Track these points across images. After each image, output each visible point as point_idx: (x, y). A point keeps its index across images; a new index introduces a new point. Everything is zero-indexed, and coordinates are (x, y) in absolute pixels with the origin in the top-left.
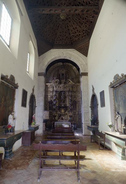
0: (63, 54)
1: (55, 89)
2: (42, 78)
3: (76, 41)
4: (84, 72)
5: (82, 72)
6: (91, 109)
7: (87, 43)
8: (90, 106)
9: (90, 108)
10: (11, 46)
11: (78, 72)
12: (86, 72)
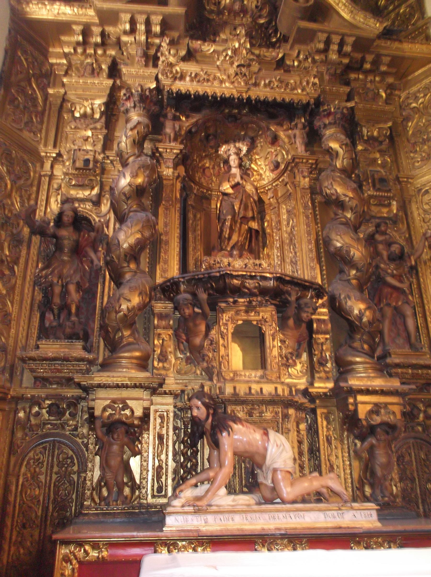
1: (138, 76)
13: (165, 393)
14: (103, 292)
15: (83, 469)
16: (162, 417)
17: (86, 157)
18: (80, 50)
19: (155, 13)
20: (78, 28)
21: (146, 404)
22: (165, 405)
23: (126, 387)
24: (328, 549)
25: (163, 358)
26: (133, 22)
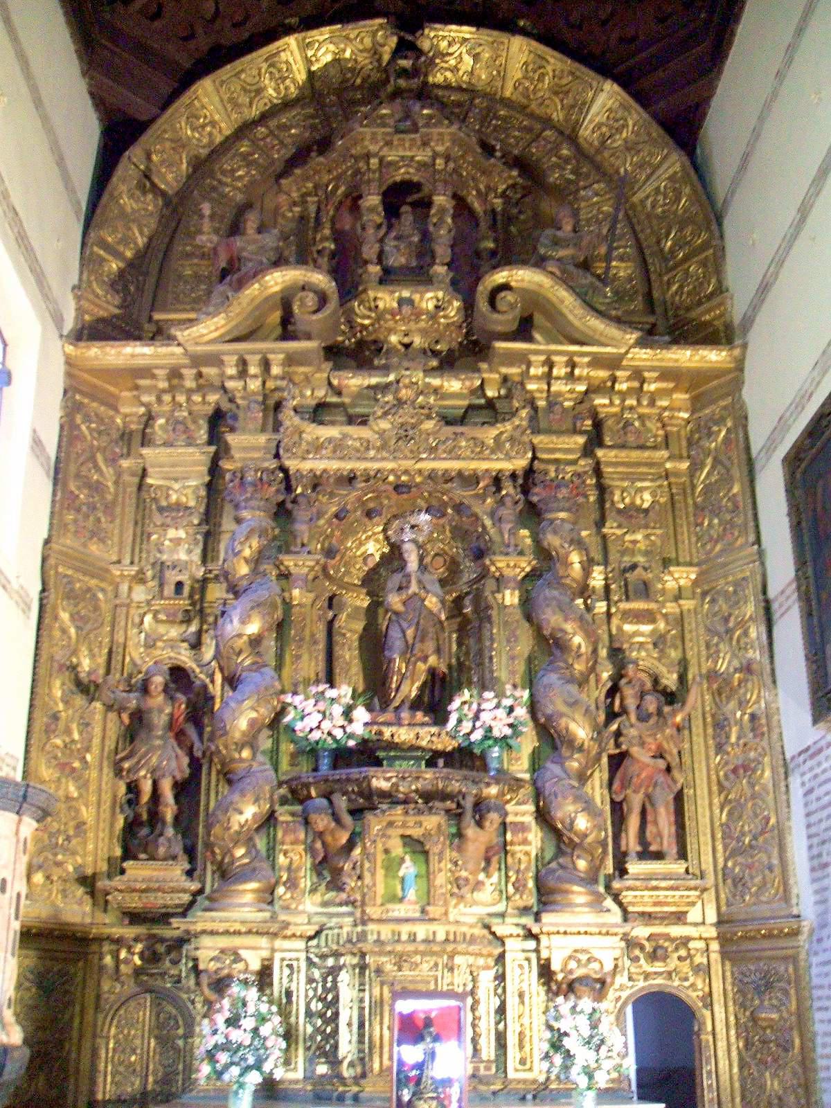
11: (675, 162)
13: (294, 935)
14: (209, 782)
16: (290, 966)
17: (179, 578)
19: (273, 352)
20: (161, 373)
21: (265, 954)
24: (730, 43)
25: (292, 884)
26: (243, 363)
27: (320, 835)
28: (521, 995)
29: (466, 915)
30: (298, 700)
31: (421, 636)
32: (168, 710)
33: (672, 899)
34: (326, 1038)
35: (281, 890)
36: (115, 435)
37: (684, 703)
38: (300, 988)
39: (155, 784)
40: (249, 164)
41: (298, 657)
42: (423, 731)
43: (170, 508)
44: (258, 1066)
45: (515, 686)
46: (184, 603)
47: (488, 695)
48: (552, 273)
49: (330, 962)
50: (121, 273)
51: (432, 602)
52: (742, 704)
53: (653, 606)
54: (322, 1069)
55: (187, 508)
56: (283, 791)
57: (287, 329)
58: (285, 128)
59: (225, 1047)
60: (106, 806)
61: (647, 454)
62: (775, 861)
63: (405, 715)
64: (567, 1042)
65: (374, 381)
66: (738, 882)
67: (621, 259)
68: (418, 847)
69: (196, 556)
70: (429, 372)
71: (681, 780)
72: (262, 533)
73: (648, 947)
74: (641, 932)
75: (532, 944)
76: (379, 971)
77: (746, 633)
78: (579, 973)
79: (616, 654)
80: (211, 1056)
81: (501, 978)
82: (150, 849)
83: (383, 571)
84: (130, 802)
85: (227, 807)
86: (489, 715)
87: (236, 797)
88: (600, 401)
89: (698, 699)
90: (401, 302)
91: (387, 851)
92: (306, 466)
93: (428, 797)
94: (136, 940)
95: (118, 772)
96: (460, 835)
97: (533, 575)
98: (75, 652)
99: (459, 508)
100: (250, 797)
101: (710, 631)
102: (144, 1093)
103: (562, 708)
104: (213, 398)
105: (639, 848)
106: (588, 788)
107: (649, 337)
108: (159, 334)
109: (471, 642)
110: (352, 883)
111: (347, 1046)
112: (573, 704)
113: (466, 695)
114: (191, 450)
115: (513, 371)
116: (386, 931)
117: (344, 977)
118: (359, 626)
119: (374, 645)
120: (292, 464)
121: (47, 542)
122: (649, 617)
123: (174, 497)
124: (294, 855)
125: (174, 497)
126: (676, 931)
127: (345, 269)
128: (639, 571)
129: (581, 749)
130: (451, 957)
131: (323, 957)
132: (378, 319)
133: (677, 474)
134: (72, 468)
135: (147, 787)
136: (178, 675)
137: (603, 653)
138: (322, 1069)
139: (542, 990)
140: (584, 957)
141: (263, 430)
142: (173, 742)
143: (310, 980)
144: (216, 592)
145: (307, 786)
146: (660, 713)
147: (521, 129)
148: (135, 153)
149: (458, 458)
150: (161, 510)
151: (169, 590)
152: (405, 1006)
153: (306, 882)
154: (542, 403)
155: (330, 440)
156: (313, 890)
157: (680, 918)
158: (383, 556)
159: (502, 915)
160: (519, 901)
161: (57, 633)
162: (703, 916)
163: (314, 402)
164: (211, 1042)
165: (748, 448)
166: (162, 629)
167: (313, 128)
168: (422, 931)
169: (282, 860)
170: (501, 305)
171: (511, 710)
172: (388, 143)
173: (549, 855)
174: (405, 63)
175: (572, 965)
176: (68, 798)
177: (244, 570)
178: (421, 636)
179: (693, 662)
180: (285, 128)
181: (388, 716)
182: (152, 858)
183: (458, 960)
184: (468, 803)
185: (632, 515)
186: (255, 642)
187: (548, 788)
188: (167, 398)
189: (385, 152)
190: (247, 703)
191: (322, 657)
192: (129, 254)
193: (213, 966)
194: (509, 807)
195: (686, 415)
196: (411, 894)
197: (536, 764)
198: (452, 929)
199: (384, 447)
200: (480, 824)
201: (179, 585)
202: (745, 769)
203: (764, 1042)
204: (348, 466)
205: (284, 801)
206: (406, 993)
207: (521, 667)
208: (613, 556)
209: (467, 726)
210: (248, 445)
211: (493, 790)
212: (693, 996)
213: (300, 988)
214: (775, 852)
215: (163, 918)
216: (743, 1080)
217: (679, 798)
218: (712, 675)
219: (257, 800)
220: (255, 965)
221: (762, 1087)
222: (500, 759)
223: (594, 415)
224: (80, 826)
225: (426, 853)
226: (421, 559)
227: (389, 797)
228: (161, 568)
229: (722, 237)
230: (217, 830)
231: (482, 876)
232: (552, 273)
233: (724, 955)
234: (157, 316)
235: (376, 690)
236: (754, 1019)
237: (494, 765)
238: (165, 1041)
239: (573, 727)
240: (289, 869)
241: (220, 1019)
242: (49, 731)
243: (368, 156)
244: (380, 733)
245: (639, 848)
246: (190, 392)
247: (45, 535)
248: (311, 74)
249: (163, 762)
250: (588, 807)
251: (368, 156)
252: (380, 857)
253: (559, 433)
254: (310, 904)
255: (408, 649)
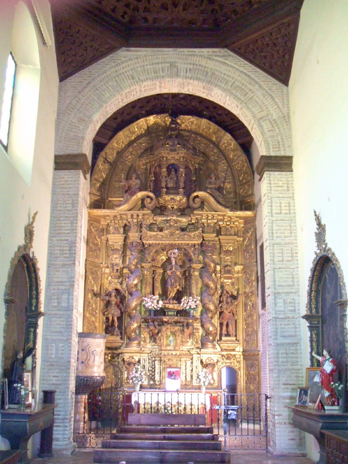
0: (175, 70)
2: (83, 186)
3: (235, 12)
4: (272, 154)
5: (264, 154)
6: (311, 328)
7: (285, 20)
8: (304, 311)
9: (305, 324)
10: (12, 149)
11: (244, 157)
12: (282, 153)
15: (122, 373)
18: (113, 221)
21: (139, 357)
22: (145, 356)
23: (133, 353)
26: (132, 216)
27: (151, 330)
28: (196, 367)
29: (185, 348)
30: (146, 299)
31: (176, 282)
32: (115, 300)
33: (232, 346)
34: (153, 376)
35: (142, 343)
36: (100, 230)
37: (237, 300)
38: (147, 365)
39: (113, 318)
40: (132, 154)
41: (146, 288)
42: (175, 305)
43: (114, 250)
44: (141, 381)
45: (197, 295)
46: (118, 274)
47: (191, 298)
48: (209, 193)
49: (153, 359)
50: (100, 186)
51: (178, 273)
52: (251, 301)
53: (231, 275)
54: (152, 382)
55: (118, 250)
56: (143, 320)
57: (143, 206)
58: (141, 143)
59: (135, 377)
60: (101, 323)
61: (232, 237)
62: (255, 338)
63: (171, 301)
64: (200, 377)
65: (164, 219)
66: (247, 342)
67: (229, 182)
68: (174, 334)
69: (121, 262)
70: (177, 216)
71: (236, 318)
72: (137, 259)
73: (226, 356)
74: (225, 353)
75: (199, 356)
76: (164, 361)
77: (252, 284)
78: (209, 362)
79: (222, 287)
80: (132, 379)
81: (192, 363)
82: (112, 332)
83: (166, 263)
84: (106, 322)
85: (130, 324)
86: (190, 303)
87: (132, 322)
88: (220, 223)
89: (241, 299)
90: (171, 199)
91: (167, 334)
92: (148, 242)
93: (176, 322)
94: (109, 353)
95: (104, 314)
96: (183, 330)
97: (202, 268)
98: (93, 287)
99: (185, 249)
100: (135, 322)
101: (245, 282)
102: (112, 387)
103: (208, 302)
104: (125, 222)
105: (226, 333)
106: (213, 321)
107: (233, 209)
108: (111, 206)
109: (188, 282)
110: (158, 342)
111: (157, 378)
112: (210, 301)
113: (185, 298)
114: (119, 235)
115: (199, 217)
116: (166, 353)
117: (157, 362)
118: (160, 277)
119: (164, 282)
120: (144, 242)
121: (86, 260)
122: (230, 278)
123: (115, 247)
124: (145, 335)
125: (115, 247)
126: (233, 353)
127: (157, 192)
128: (228, 267)
129: (211, 311)
130: (180, 358)
131: (152, 358)
132: (166, 202)
133: (240, 241)
134: (91, 241)
135: (111, 318)
136: (117, 290)
137: (219, 287)
138: (152, 382)
139: (201, 366)
140: (210, 359)
141: (137, 232)
142: (117, 308)
143: (149, 363)
144: (125, 271)
145: (148, 319)
146: (231, 302)
147: (204, 144)
148: (103, 154)
149: (184, 240)
150: (112, 250)
151: (115, 271)
152: (169, 370)
153: (148, 341)
154: (206, 225)
155: (154, 235)
156: (150, 343)
157: (234, 350)
158: (167, 259)
159: (193, 349)
160: (197, 346)
161: (89, 282)
162: (239, 349)
163: (149, 224)
164: (132, 376)
165: (256, 237)
166: (113, 280)
167: (149, 143)
168: (174, 353)
169: (142, 336)
170: (195, 202)
171: (196, 301)
172: (169, 154)
173: (204, 335)
174: (173, 126)
175: (207, 361)
176: (93, 321)
177: (133, 267)
178: (176, 282)
179: (241, 289)
180: (141, 143)
181: (167, 301)
182: (113, 335)
183: (182, 359)
184: (185, 324)
185: (228, 252)
186: (136, 285)
187: (204, 320)
188: (113, 221)
189: (168, 156)
190: (135, 300)
191: (151, 288)
192: (101, 180)
193: (128, 360)
194: (194, 324)
195: (242, 225)
196: (172, 344)
197: (202, 315)
198: (181, 352)
199: (167, 237)
200: (188, 328)
201: (117, 270)
202: (250, 316)
203: (251, 378)
204: (158, 242)
205: (143, 322)
206: (170, 367)
207: (199, 291)
208: (223, 263)
209: (185, 305)
210: (134, 236)
211: (191, 321)
212: (236, 368)
213: (147, 365)
214: (255, 336)
215: (116, 349)
216: (246, 387)
217: (236, 321)
218: (245, 292)
219: (137, 323)
220: (137, 360)
221: (250, 388)
222: (193, 313)
223: (219, 225)
224: (96, 327)
225: (175, 335)
226: (176, 261)
227: (167, 322)
228: (113, 265)
229: (254, 179)
230: (128, 329)
231: (188, 340)
232: (209, 193)
233: (244, 359)
234: (110, 199)
235: (164, 295)
236: (249, 373)
237: (192, 314)
238: (116, 376)
239: (210, 306)
240: (144, 338)
241: (134, 372)
242: (88, 306)
243: (163, 157)
244: (165, 306)
245: (226, 333)
246: (119, 220)
247: (85, 258)
248: (148, 127)
249: (114, 312)
250: (213, 325)
251: (163, 157)
252: (165, 335)
253: (210, 233)
254: (149, 346)
255: (172, 285)
